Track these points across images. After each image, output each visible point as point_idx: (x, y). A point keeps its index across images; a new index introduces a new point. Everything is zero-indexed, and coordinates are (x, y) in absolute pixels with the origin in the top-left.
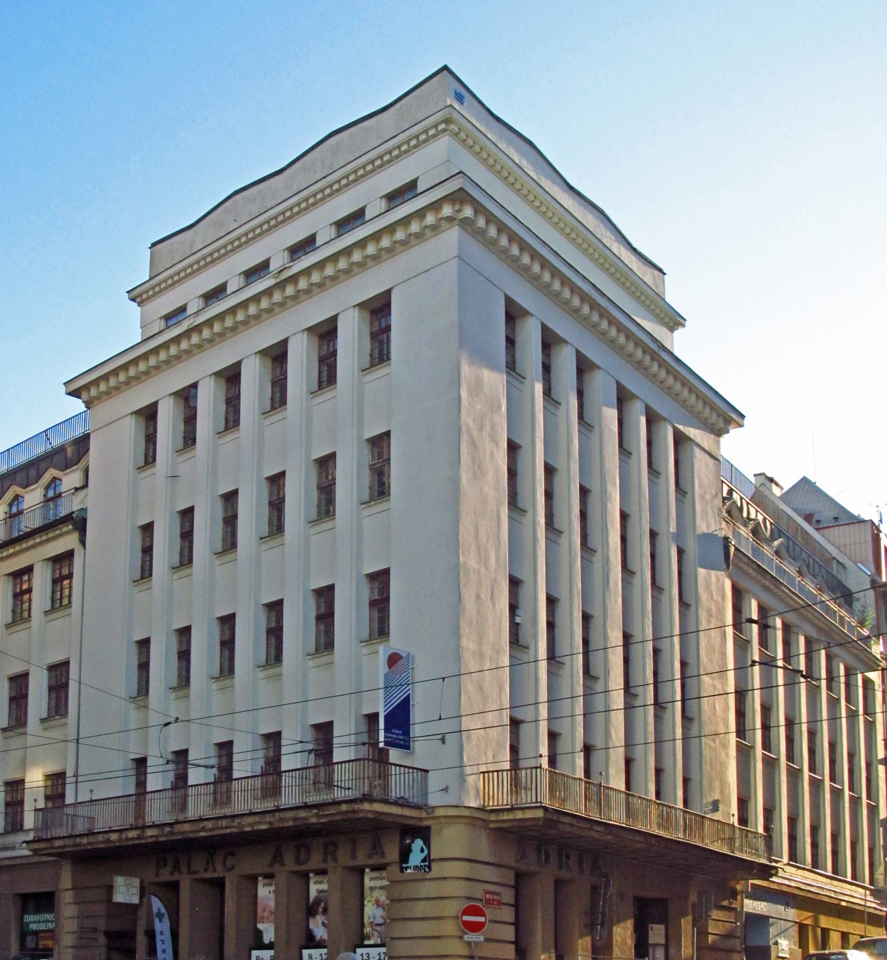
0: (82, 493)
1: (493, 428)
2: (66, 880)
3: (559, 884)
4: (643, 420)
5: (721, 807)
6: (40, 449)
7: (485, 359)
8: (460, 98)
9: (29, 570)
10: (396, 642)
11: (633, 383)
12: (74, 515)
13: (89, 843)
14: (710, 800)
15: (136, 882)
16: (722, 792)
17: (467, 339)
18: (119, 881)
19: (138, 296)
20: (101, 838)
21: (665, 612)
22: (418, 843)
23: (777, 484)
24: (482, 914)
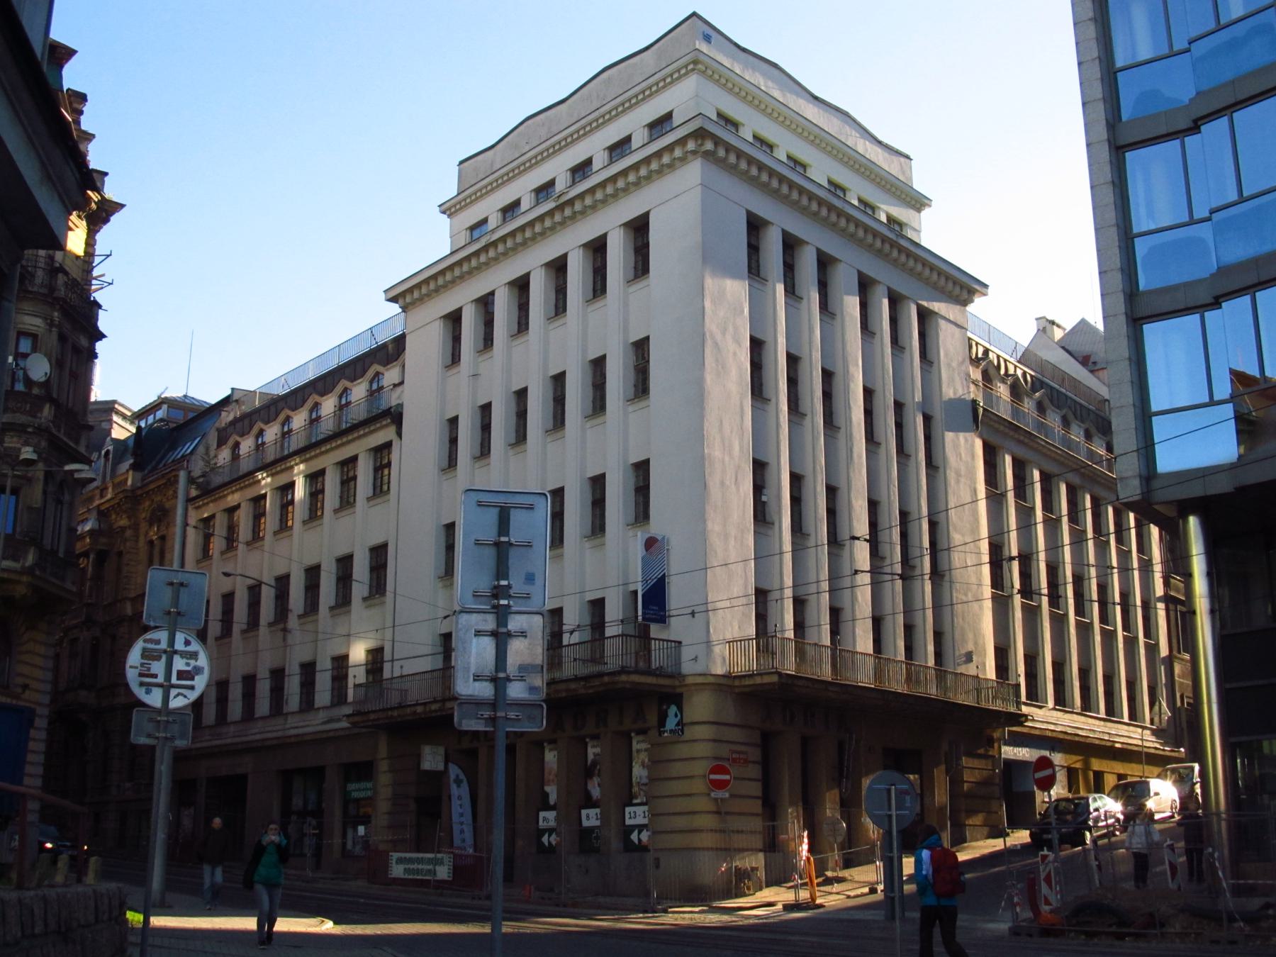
0: (399, 390)
1: (736, 328)
2: (383, 750)
3: (805, 741)
4: (886, 302)
5: (974, 658)
6: (363, 347)
7: (726, 270)
8: (707, 39)
9: (354, 459)
10: (656, 527)
11: (874, 269)
14: (963, 652)
15: (441, 750)
16: (976, 643)
17: (710, 258)
18: (427, 751)
19: (449, 209)
20: (408, 710)
21: (912, 477)
23: (1059, 326)
24: (727, 772)
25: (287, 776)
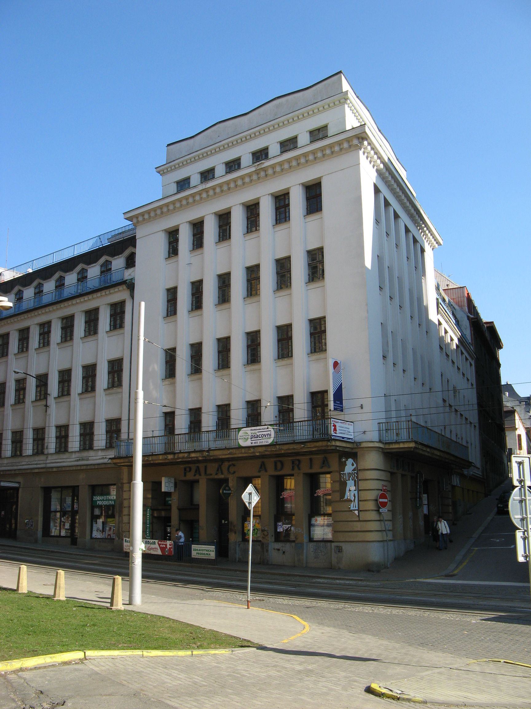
12: (128, 281)
13: (152, 460)
19: (162, 171)
22: (350, 461)
25: (47, 491)
